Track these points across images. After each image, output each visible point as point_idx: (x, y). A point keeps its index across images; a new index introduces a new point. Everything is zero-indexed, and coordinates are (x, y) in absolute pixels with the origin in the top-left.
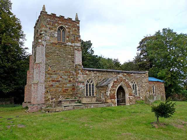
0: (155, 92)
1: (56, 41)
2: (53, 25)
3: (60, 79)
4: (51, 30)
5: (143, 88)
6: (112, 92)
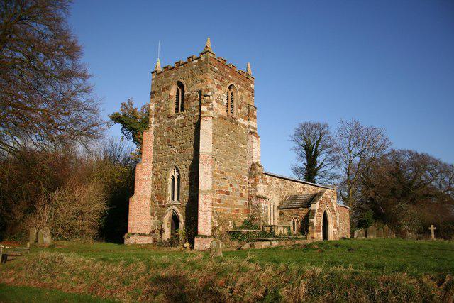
3: (230, 189)
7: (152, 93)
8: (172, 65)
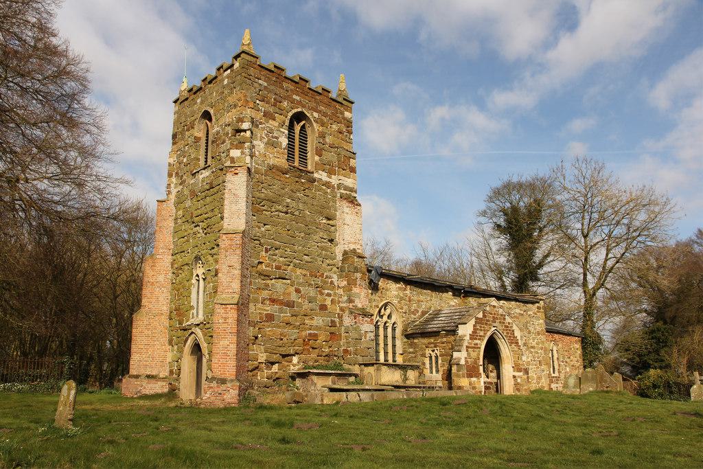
0: (556, 367)
1: (282, 162)
2: (275, 105)
3: (294, 297)
4: (271, 122)
5: (531, 352)
6: (472, 353)
7: (174, 136)
8: (199, 84)
